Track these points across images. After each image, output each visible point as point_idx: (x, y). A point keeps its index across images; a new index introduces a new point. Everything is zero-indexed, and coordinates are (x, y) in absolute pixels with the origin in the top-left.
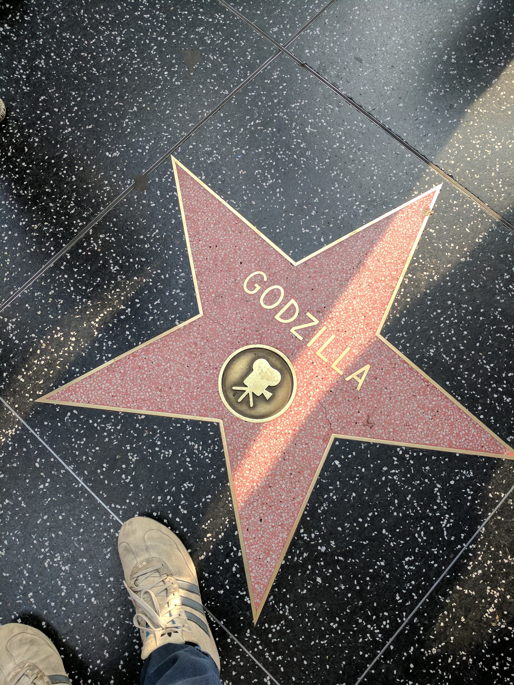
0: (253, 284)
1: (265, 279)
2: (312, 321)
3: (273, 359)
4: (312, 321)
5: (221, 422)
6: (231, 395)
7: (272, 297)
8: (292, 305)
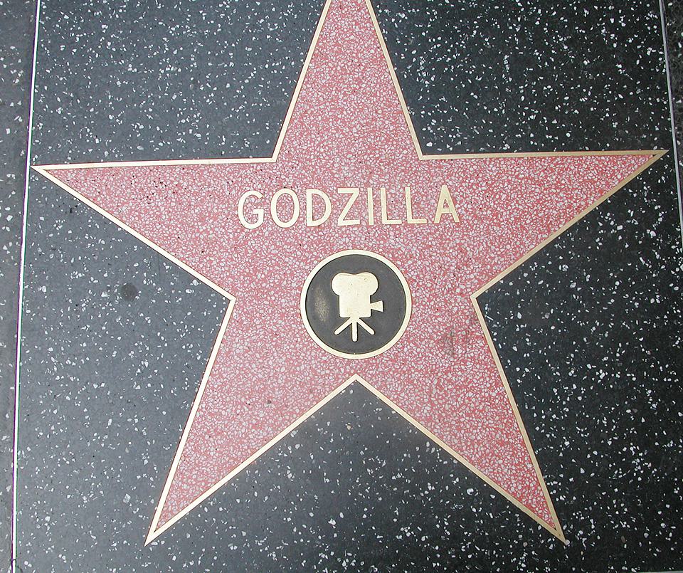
1: (260, 196)
4: (349, 216)
5: (356, 377)
7: (285, 207)
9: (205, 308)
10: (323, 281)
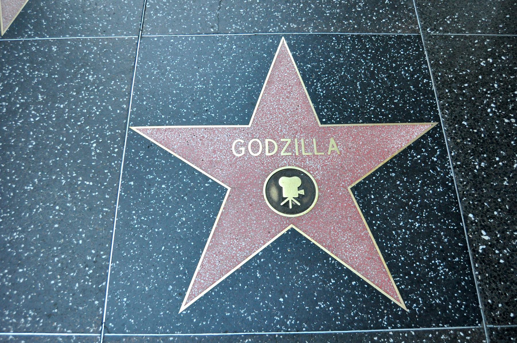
2: (287, 142)
7: (255, 147)
8: (269, 142)
9: (360, 190)
10: (276, 178)
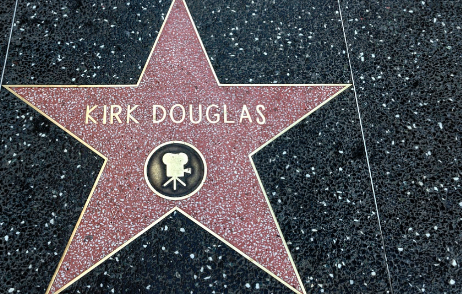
0: (113, 113)
3: (171, 149)
5: (219, 84)
6: (168, 191)
